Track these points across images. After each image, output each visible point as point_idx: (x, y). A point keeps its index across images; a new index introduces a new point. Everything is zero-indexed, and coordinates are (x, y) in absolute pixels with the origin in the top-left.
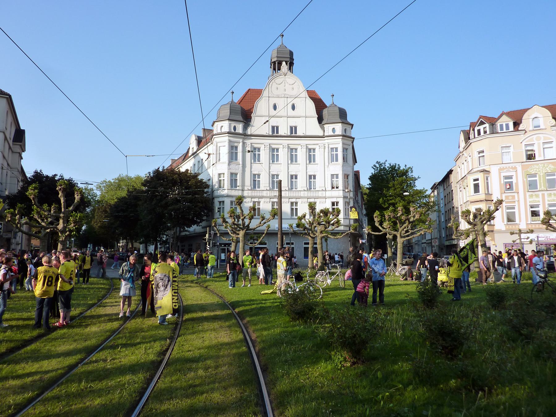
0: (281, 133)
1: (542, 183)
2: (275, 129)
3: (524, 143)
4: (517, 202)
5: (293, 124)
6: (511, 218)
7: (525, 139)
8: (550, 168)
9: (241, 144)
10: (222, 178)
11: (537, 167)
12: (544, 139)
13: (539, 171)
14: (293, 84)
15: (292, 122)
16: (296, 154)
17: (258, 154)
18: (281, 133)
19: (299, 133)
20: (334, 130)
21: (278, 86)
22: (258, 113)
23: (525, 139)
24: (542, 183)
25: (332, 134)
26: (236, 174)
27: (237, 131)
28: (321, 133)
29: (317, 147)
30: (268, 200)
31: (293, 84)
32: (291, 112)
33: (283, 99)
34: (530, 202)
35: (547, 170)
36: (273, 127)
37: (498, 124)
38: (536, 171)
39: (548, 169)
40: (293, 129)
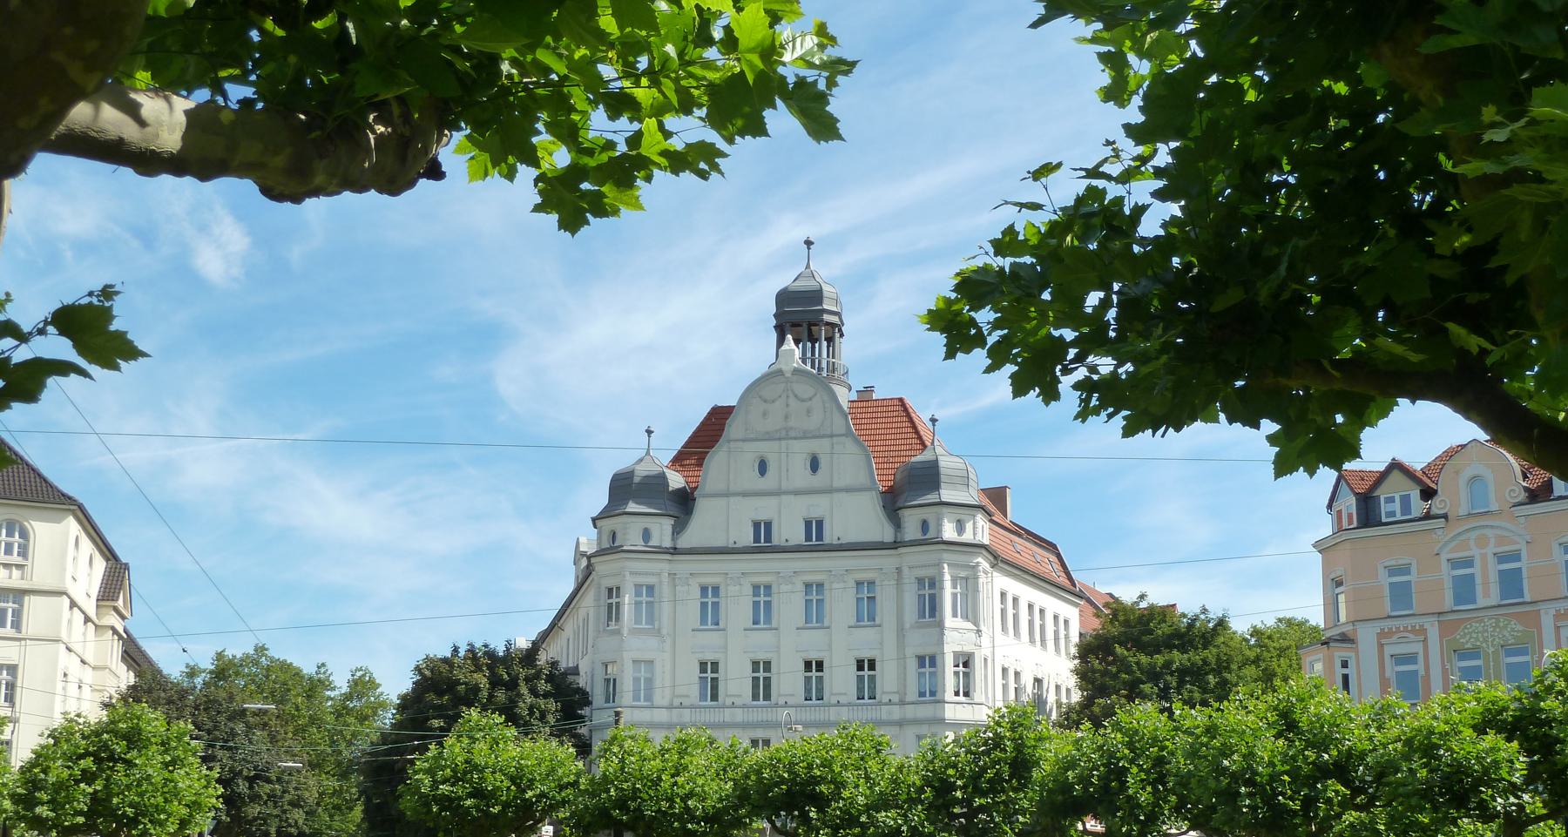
2: (763, 529)
8: (1513, 630)
11: (1480, 629)
12: (1501, 540)
14: (810, 399)
19: (828, 538)
20: (646, 535)
21: (808, 404)
25: (919, 536)
38: (1477, 639)
40: (814, 527)
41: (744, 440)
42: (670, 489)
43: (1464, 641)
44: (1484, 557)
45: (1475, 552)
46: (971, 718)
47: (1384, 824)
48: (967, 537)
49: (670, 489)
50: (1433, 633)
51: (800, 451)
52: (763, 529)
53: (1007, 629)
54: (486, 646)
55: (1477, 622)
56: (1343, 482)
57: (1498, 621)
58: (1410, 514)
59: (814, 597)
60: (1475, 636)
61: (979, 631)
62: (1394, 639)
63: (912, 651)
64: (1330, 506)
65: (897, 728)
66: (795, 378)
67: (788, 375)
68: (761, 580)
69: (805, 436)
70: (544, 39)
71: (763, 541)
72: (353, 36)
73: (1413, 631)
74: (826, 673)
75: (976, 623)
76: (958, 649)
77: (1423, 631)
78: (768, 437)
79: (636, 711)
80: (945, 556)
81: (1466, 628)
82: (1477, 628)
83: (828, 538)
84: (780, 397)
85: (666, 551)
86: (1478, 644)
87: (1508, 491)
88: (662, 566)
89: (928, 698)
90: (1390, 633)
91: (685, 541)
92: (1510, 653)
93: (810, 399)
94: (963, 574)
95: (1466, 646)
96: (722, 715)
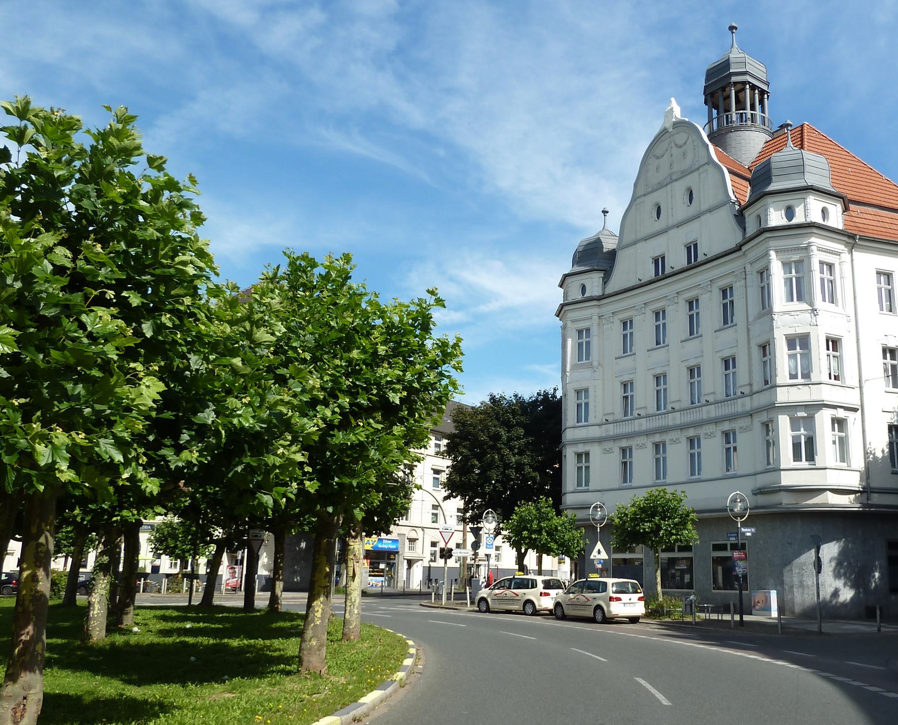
2: (659, 262)
14: (685, 143)
25: (579, 297)
41: (645, 195)
42: (605, 250)
46: (808, 399)
47: (474, 472)
48: (799, 219)
49: (605, 250)
51: (679, 188)
52: (659, 262)
53: (837, 299)
54: (516, 396)
56: (624, 243)
59: (584, 340)
61: (814, 311)
63: (756, 341)
64: (561, 286)
65: (749, 419)
66: (675, 130)
67: (671, 130)
68: (583, 325)
69: (672, 180)
70: (7, 547)
75: (811, 304)
76: (791, 331)
78: (684, 174)
79: (577, 430)
80: (772, 243)
84: (667, 150)
85: (599, 299)
88: (591, 311)
89: (800, 380)
91: (611, 288)
93: (685, 143)
94: (796, 257)
96: (633, 426)
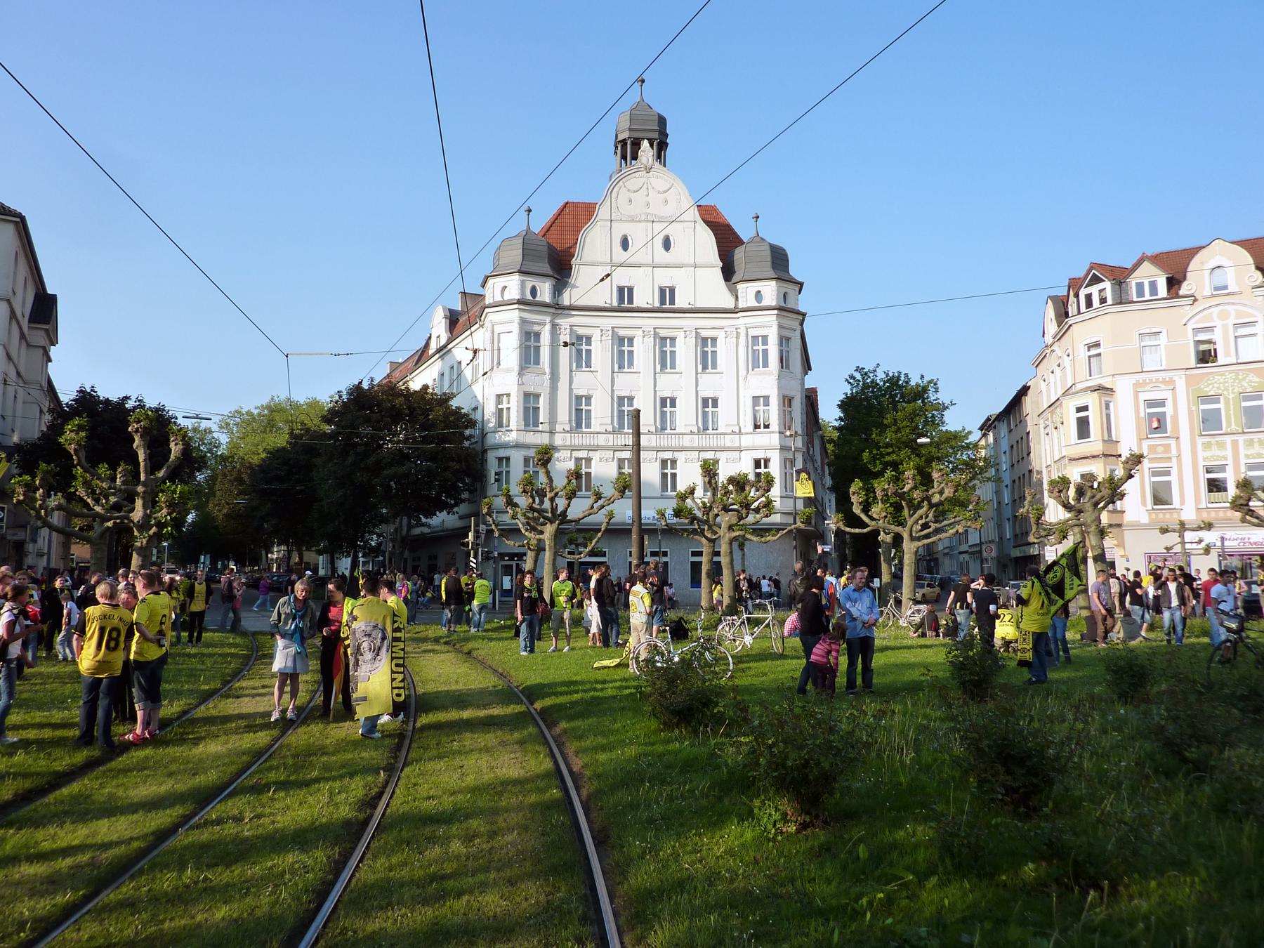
0: (639, 302)
1: (1232, 416)
2: (625, 293)
3: (1191, 326)
4: (1174, 460)
5: (667, 283)
6: (1162, 495)
7: (1193, 316)
8: (1251, 381)
9: (548, 328)
10: (504, 406)
11: (1222, 381)
12: (1237, 316)
13: (1226, 389)
14: (665, 192)
15: (664, 278)
16: (673, 349)
17: (586, 350)
18: (639, 302)
19: (680, 302)
20: (758, 295)
21: (633, 196)
22: (586, 258)
23: (1193, 316)
24: (1232, 416)
25: (755, 304)
26: (537, 396)
27: (538, 298)
28: (729, 303)
29: (720, 335)
30: (610, 454)
31: (665, 192)
32: (661, 255)
33: (644, 224)
34: (1205, 459)
35: (1242, 386)
36: (621, 290)
37: (1133, 282)
38: (1219, 388)
39: (1246, 385)
40: (667, 294)
43: (1208, 389)
44: (1225, 327)
45: (1217, 322)
50: (1181, 384)
55: (1218, 375)
57: (1237, 375)
58: (1157, 295)
60: (1216, 385)
62: (1148, 388)
71: (625, 300)
72: (860, 660)
73: (1164, 382)
74: (677, 409)
77: (1172, 381)
81: (1208, 380)
82: (1219, 380)
83: (680, 302)
86: (1220, 391)
87: (1246, 278)
90: (1145, 383)
92: (1245, 399)
95: (1210, 394)
